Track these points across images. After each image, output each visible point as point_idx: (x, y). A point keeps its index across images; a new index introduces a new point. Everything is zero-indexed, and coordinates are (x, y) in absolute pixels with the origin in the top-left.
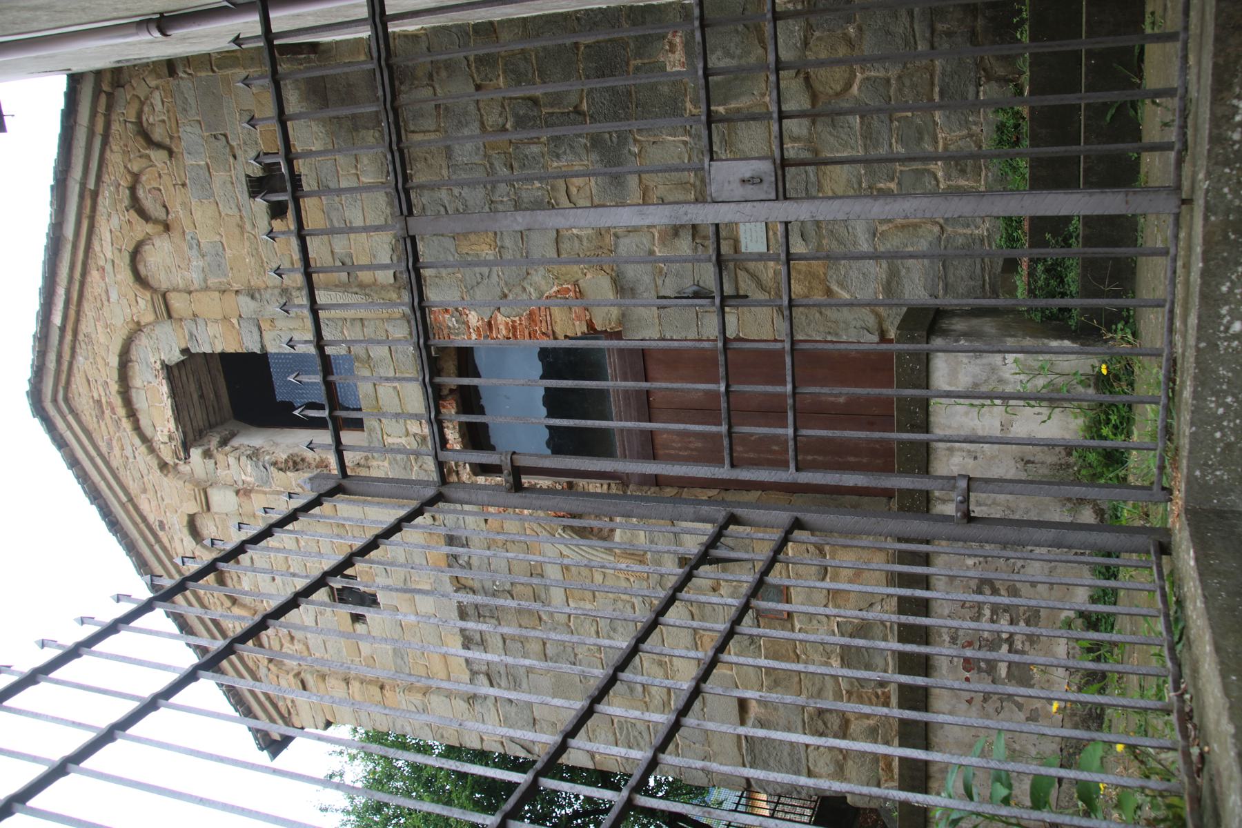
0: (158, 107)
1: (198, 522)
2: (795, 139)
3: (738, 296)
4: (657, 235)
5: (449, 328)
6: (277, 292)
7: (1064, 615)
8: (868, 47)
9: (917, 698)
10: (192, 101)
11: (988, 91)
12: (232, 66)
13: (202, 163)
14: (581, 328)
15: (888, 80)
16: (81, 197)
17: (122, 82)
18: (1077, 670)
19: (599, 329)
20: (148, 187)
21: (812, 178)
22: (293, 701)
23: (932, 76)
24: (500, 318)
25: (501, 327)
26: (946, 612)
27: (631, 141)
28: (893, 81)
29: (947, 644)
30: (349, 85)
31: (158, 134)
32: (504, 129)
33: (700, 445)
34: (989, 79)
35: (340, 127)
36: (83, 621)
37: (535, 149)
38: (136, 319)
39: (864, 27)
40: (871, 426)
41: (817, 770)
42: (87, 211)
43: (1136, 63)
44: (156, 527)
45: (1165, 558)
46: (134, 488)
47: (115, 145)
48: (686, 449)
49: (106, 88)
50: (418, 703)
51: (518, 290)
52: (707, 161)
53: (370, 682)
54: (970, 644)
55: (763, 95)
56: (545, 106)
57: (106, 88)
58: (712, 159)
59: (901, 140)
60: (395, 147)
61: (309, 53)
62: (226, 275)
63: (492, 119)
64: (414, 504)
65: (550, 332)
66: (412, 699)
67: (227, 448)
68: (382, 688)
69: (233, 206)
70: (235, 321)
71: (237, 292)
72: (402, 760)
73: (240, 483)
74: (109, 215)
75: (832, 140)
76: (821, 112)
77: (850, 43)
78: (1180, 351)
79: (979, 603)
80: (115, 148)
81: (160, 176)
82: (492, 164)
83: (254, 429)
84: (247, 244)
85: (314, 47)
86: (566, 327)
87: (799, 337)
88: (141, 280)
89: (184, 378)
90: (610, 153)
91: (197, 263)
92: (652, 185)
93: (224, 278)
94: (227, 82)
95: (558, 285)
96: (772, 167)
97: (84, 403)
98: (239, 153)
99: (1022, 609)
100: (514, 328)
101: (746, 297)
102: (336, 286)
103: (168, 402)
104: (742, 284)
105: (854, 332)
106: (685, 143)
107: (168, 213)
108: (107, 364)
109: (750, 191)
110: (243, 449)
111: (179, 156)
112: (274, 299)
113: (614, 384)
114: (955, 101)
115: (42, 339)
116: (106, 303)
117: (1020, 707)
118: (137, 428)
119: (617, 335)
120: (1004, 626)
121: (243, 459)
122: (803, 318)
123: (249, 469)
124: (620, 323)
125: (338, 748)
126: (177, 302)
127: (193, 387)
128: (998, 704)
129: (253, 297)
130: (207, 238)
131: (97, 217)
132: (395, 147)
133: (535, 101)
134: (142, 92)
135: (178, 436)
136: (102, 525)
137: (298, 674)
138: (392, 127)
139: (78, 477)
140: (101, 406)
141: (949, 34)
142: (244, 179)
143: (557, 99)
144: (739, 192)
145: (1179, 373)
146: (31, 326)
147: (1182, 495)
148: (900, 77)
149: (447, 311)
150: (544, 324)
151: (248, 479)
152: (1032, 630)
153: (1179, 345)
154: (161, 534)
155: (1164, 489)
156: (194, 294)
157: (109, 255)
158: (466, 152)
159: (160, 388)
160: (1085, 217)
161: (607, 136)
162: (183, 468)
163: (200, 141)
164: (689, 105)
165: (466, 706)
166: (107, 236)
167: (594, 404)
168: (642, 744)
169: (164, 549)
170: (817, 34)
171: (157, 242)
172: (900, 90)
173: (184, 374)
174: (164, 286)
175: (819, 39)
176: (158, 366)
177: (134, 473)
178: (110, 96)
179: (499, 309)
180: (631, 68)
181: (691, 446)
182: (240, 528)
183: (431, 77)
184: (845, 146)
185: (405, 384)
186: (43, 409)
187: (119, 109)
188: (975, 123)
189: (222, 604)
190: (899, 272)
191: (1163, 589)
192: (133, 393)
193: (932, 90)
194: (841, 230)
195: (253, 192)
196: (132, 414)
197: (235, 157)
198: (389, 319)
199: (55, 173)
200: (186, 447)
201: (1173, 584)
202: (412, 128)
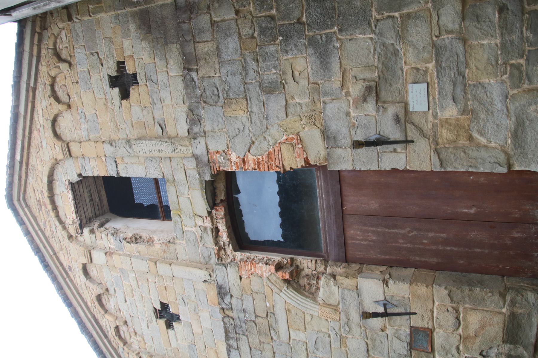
1: (88, 268)
4: (351, 101)
5: (220, 163)
10: (80, 34)
16: (27, 91)
19: (312, 163)
20: (60, 85)
25: (251, 162)
27: (335, 39)
30: (163, 18)
31: (64, 55)
32: (252, 37)
33: (374, 238)
35: (158, 43)
42: (30, 98)
46: (56, 247)
47: (43, 62)
49: (38, 30)
51: (261, 138)
56: (279, 20)
57: (38, 30)
67: (102, 229)
69: (102, 93)
70: (103, 158)
71: (103, 142)
73: (108, 249)
80: (44, 63)
81: (66, 78)
82: (245, 60)
83: (120, 218)
84: (109, 114)
86: (292, 161)
88: (57, 135)
90: (322, 53)
91: (84, 126)
92: (348, 68)
94: (98, 21)
97: (32, 202)
98: (104, 62)
100: (259, 162)
102: (156, 138)
103: (72, 203)
104: (410, 134)
106: (371, 39)
107: (70, 98)
108: (42, 182)
111: (75, 66)
115: (11, 167)
116: (41, 149)
118: (58, 216)
121: (109, 235)
122: (452, 156)
123: (112, 241)
124: (326, 160)
126: (74, 147)
127: (86, 195)
129: (111, 145)
130: (89, 111)
134: (56, 31)
135: (77, 221)
137: (138, 354)
139: (29, 241)
140: (40, 204)
142: (107, 77)
151: (112, 246)
154: (70, 273)
156: (82, 143)
157: (42, 123)
159: (68, 195)
161: (319, 37)
162: (80, 238)
164: (374, 13)
166: (40, 112)
173: (81, 187)
176: (67, 183)
178: (40, 34)
181: (369, 238)
186: (14, 205)
187: (45, 42)
189: (100, 312)
190: (524, 123)
195: (112, 85)
196: (55, 208)
197: (102, 65)
199: (14, 78)
200: (82, 227)
202: (198, 40)
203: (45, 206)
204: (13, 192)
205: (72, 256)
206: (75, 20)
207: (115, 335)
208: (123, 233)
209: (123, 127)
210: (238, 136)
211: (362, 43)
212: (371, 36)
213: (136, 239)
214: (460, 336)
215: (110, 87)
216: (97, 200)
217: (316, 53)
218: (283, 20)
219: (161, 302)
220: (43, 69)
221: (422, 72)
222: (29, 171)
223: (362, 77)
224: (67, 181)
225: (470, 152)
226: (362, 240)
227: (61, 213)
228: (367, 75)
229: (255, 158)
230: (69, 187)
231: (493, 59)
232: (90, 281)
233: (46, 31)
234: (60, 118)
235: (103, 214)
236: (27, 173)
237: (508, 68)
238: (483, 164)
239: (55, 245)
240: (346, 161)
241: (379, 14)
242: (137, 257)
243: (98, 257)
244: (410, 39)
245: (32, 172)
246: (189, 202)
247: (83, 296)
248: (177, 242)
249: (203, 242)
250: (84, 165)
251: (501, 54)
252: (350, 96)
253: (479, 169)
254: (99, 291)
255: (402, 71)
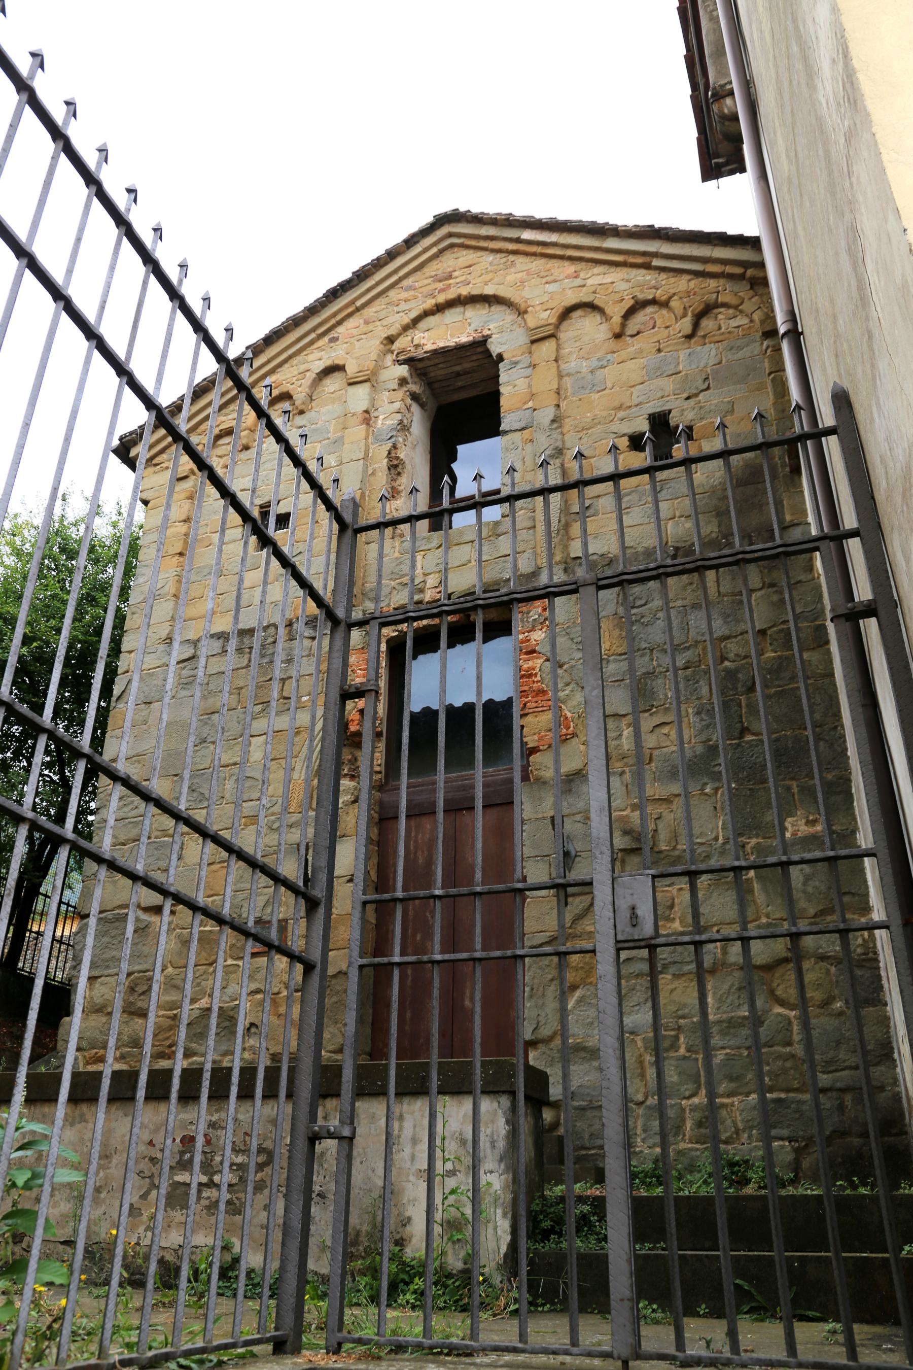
0: (734, 323)
2: (725, 952)
3: (566, 896)
4: (624, 813)
5: (528, 613)
6: (559, 444)
7: (236, 1242)
8: (821, 1023)
9: (158, 1090)
10: (741, 354)
11: (783, 1149)
12: (776, 393)
13: (681, 367)
14: (531, 741)
15: (789, 1044)
16: (644, 254)
17: (756, 288)
18: (180, 1258)
19: (531, 758)
20: (656, 316)
21: (687, 968)
22: (167, 468)
23: (797, 1090)
24: (538, 662)
25: (530, 663)
26: (241, 1117)
27: (716, 785)
28: (788, 1049)
29: (209, 1117)
31: (707, 324)
32: (723, 659)
33: (420, 861)
34: (798, 1151)
35: (720, 499)
36: (206, 300)
37: (705, 691)
38: (530, 309)
39: (843, 1018)
40: (443, 1034)
41: (97, 985)
42: (631, 260)
43: (763, 1310)
44: (333, 334)
45: (270, 1347)
46: (369, 312)
48: (416, 848)
49: (750, 272)
50: (167, 588)
51: (567, 679)
52: (652, 872)
53: (186, 543)
54: (208, 1142)
55: (767, 916)
56: (748, 699)
57: (750, 272)
58: (654, 877)
59: (729, 1058)
60: (661, 571)
61: (791, 466)
62: (574, 394)
63: (732, 648)
64: (328, 597)
65: (527, 711)
66: (170, 583)
67: (409, 401)
68: (181, 554)
69: (640, 399)
70: (530, 404)
71: (558, 406)
72: (115, 573)
73: (375, 414)
74: (628, 281)
75: (726, 987)
76: (754, 976)
77: (826, 1003)
78: (478, 1360)
79: (249, 1150)
80: (692, 283)
81: (667, 327)
82: (688, 648)
83: (428, 425)
84: (605, 414)
85: (796, 470)
86: (533, 727)
87: (527, 959)
88: (567, 313)
89: (475, 358)
90: (700, 766)
91: (585, 366)
92: (674, 807)
93: (579, 391)
94: (760, 387)
95: (573, 718)
96: (647, 936)
97: (449, 262)
98: (692, 402)
99: (242, 1195)
100: (530, 676)
101: (566, 905)
102: (566, 502)
103: (451, 342)
104: (578, 900)
105: (535, 1013)
106: (716, 839)
107: (632, 336)
108: (486, 283)
109: (624, 915)
110: (408, 416)
111: (687, 345)
112: (552, 441)
113: (479, 774)
114: (768, 1118)
115: (509, 222)
116: (544, 280)
117: (144, 1197)
118: (426, 314)
119: (525, 778)
120: (226, 1177)
121: (399, 416)
123: (389, 422)
124: (538, 779)
125: (125, 511)
126: (547, 348)
127: (467, 365)
128: (147, 1174)
129: (553, 421)
130: (610, 374)
131: (625, 270)
132: (661, 571)
133: (751, 689)
134: (747, 307)
135: (420, 353)
136: (333, 283)
138: (680, 568)
140: (446, 279)
141: (841, 1108)
143: (753, 710)
144: (623, 905)
145: (456, 1359)
146: (520, 211)
147: (331, 1365)
148: (793, 1056)
149: (545, 610)
150: (534, 705)
151: (380, 422)
152: (222, 1206)
153: (486, 1360)
154: (326, 339)
155: (340, 1345)
156: (555, 364)
157: (590, 282)
158: (697, 621)
160: (606, 1256)
162: (390, 358)
163: (702, 365)
164: (753, 841)
165: (164, 636)
167: (460, 752)
168: (125, 809)
169: (312, 343)
170: (833, 969)
171: (604, 327)
172: (780, 1057)
173: (479, 359)
174: (562, 335)
175: (828, 972)
177: (384, 312)
178: (742, 277)
179: (548, 660)
180: (788, 782)
181: (419, 853)
182: (302, 436)
183: (772, 585)
184: (720, 1000)
185: (475, 570)
186: (442, 225)
187: (729, 286)
188: (750, 1137)
191: (234, 1345)
192: (459, 309)
193: (782, 1090)
194: (636, 999)
196: (439, 309)
197: (688, 398)
198: (535, 554)
199: (666, 229)
200: (410, 361)
201: (242, 1357)
203: (442, 291)
204: (465, 225)
205: (356, 343)
206: (765, 343)
207: (221, 427)
208: (404, 440)
209: (584, 440)
210: (570, 642)
211: (710, 826)
212: (721, 838)
213: (395, 467)
214: (278, 993)
215: (650, 415)
216: (460, 384)
217: (696, 757)
218: (747, 706)
219: (289, 514)
220: (683, 283)
221: (667, 913)
222: (503, 255)
223: (660, 827)
224: (489, 332)
225: (552, 988)
226: (416, 842)
227: (431, 320)
228: (663, 835)
229: (537, 670)
230: (478, 336)
231: (687, 1011)
232: (314, 380)
233: (748, 287)
234: (598, 317)
235: (434, 393)
236: (499, 251)
237: (672, 1033)
238: (536, 1006)
239: (374, 310)
240: (530, 808)
241: (752, 848)
242: (365, 471)
243: (359, 397)
244: (715, 894)
245: (504, 260)
246: (464, 561)
247: (286, 365)
248: (397, 543)
249: (400, 587)
250: (518, 367)
251: (693, 1023)
252: (632, 811)
253: (529, 1001)
254: (299, 397)
255: (669, 886)
